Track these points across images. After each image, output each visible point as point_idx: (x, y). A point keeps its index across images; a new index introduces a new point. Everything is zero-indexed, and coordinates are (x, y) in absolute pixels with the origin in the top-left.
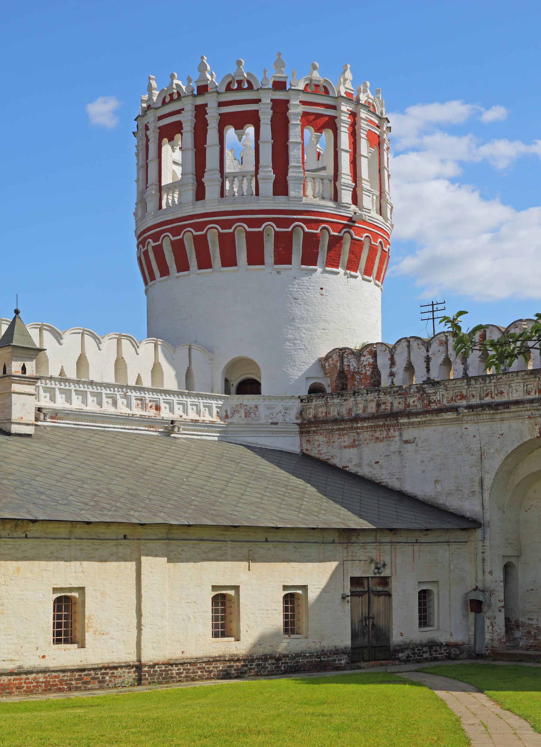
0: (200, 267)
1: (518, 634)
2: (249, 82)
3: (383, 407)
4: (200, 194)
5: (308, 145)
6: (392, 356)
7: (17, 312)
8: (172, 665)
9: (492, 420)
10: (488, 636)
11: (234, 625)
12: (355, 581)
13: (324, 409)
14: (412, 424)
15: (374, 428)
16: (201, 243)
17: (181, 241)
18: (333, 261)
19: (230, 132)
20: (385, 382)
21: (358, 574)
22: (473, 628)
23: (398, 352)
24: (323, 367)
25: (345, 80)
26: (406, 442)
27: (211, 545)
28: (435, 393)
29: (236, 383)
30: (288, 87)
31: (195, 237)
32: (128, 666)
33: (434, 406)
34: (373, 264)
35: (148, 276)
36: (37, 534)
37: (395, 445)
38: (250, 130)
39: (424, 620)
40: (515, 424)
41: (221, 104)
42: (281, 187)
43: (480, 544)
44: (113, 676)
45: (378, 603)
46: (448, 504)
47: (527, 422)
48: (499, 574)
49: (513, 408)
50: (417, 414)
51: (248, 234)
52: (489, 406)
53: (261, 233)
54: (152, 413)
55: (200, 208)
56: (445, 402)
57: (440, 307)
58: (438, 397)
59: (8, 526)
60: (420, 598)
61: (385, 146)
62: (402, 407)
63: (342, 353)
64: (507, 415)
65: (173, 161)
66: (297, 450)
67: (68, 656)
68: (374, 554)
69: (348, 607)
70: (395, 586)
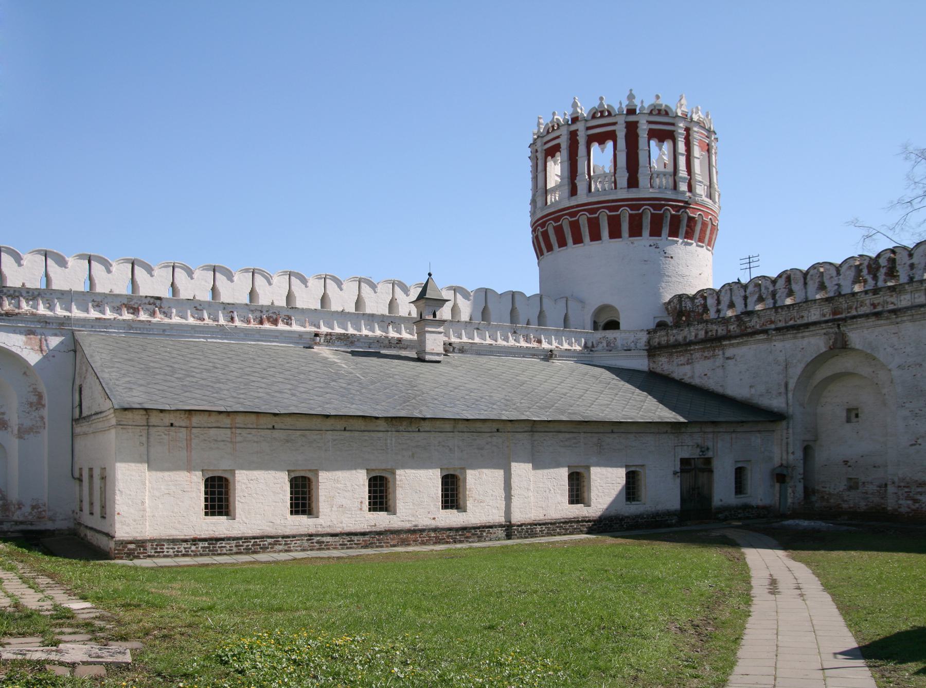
1: (814, 499)
2: (609, 112)
3: (710, 333)
4: (573, 191)
5: (658, 155)
6: (718, 297)
7: (430, 275)
8: (536, 525)
9: (795, 338)
10: (790, 500)
11: (586, 495)
12: (684, 462)
13: (665, 338)
14: (732, 345)
15: (703, 350)
16: (575, 226)
17: (561, 227)
18: (674, 233)
19: (595, 147)
20: (712, 314)
21: (686, 455)
22: (778, 495)
23: (723, 294)
24: (667, 309)
25: (681, 105)
26: (728, 358)
27: (567, 435)
28: (750, 321)
29: (602, 324)
30: (638, 112)
31: (570, 222)
32: (501, 526)
33: (749, 330)
34: (705, 234)
35: (539, 253)
36: (428, 429)
37: (719, 361)
38: (610, 144)
39: (740, 488)
40: (813, 340)
41: (588, 128)
42: (633, 182)
43: (785, 431)
44: (489, 532)
46: (760, 403)
47: (823, 337)
48: (799, 454)
49: (812, 328)
50: (736, 337)
51: (609, 217)
52: (793, 327)
53: (619, 215)
54: (535, 345)
55: (574, 202)
56: (758, 327)
57: (755, 259)
58: (752, 323)
59: (405, 423)
60: (736, 473)
61: (713, 151)
62: (724, 332)
63: (680, 297)
64: (807, 334)
65: (555, 171)
66: (646, 368)
67: (452, 518)
68: (699, 441)
69: (678, 481)
70: (717, 465)
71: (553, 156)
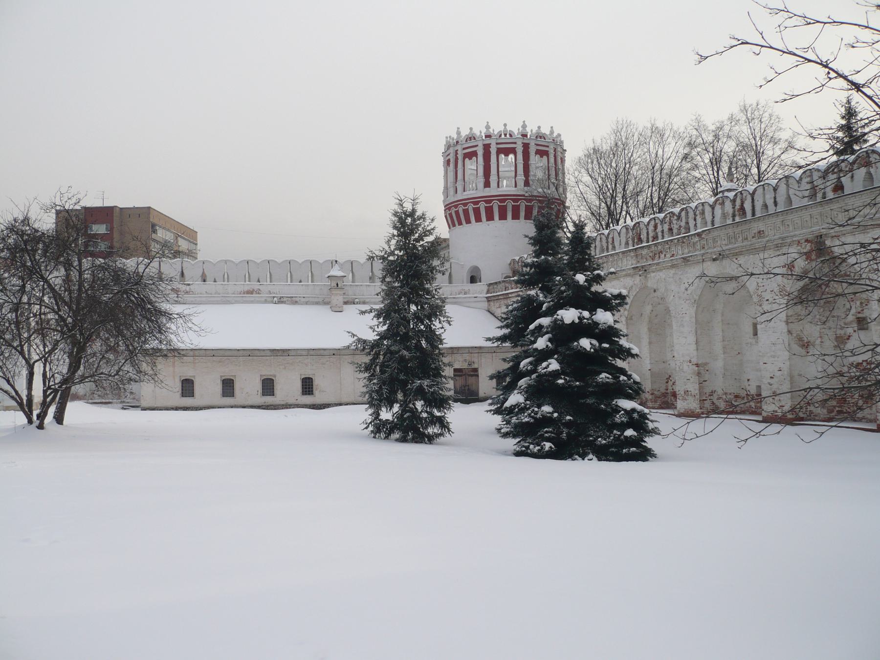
0: (500, 219)
38: (474, 158)
41: (464, 149)
45: (471, 380)
55: (488, 192)
71: (470, 159)
